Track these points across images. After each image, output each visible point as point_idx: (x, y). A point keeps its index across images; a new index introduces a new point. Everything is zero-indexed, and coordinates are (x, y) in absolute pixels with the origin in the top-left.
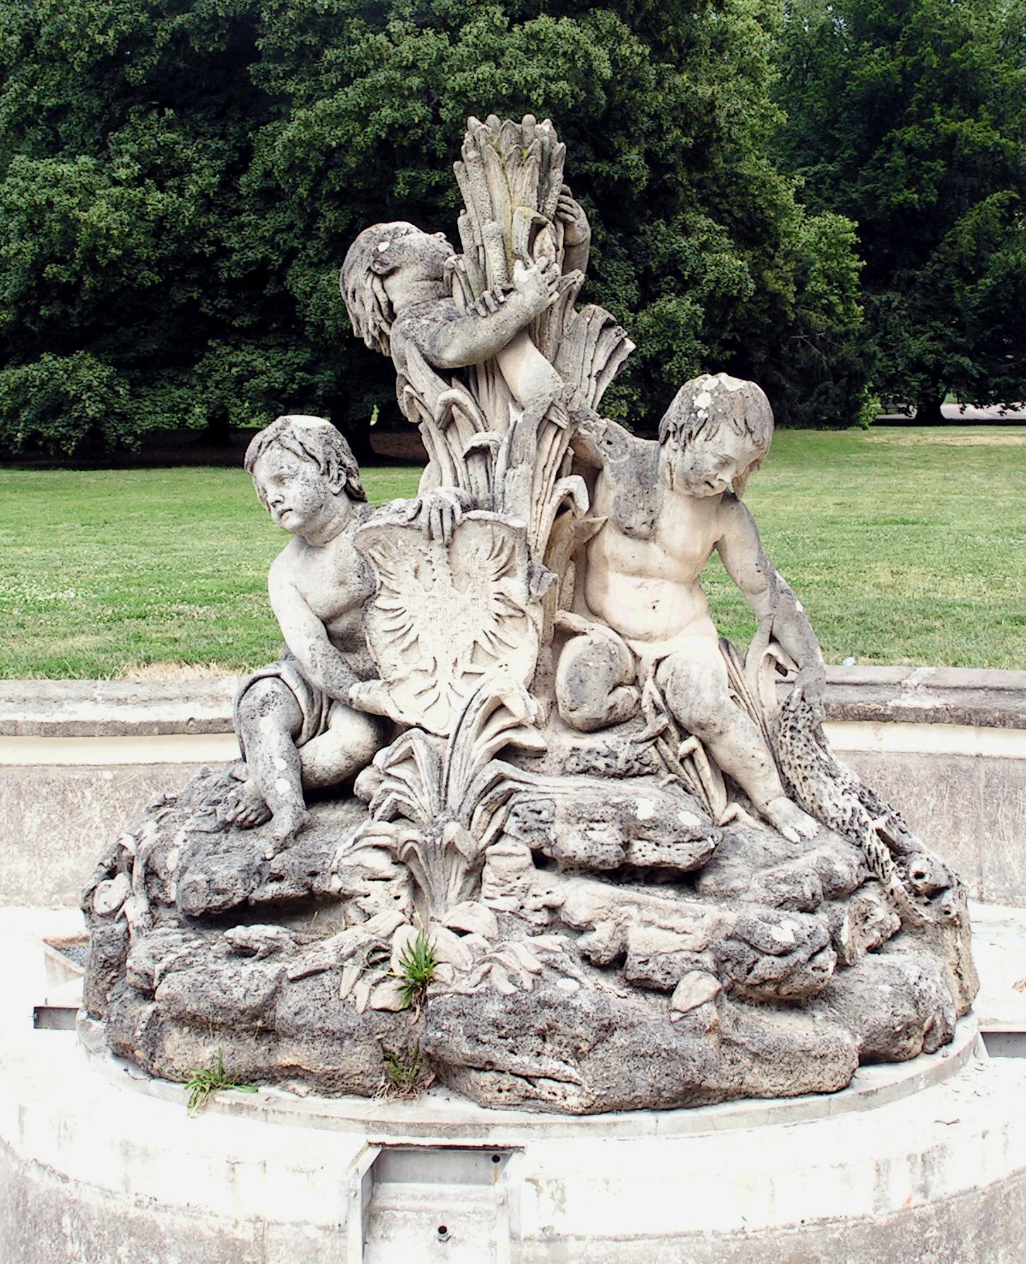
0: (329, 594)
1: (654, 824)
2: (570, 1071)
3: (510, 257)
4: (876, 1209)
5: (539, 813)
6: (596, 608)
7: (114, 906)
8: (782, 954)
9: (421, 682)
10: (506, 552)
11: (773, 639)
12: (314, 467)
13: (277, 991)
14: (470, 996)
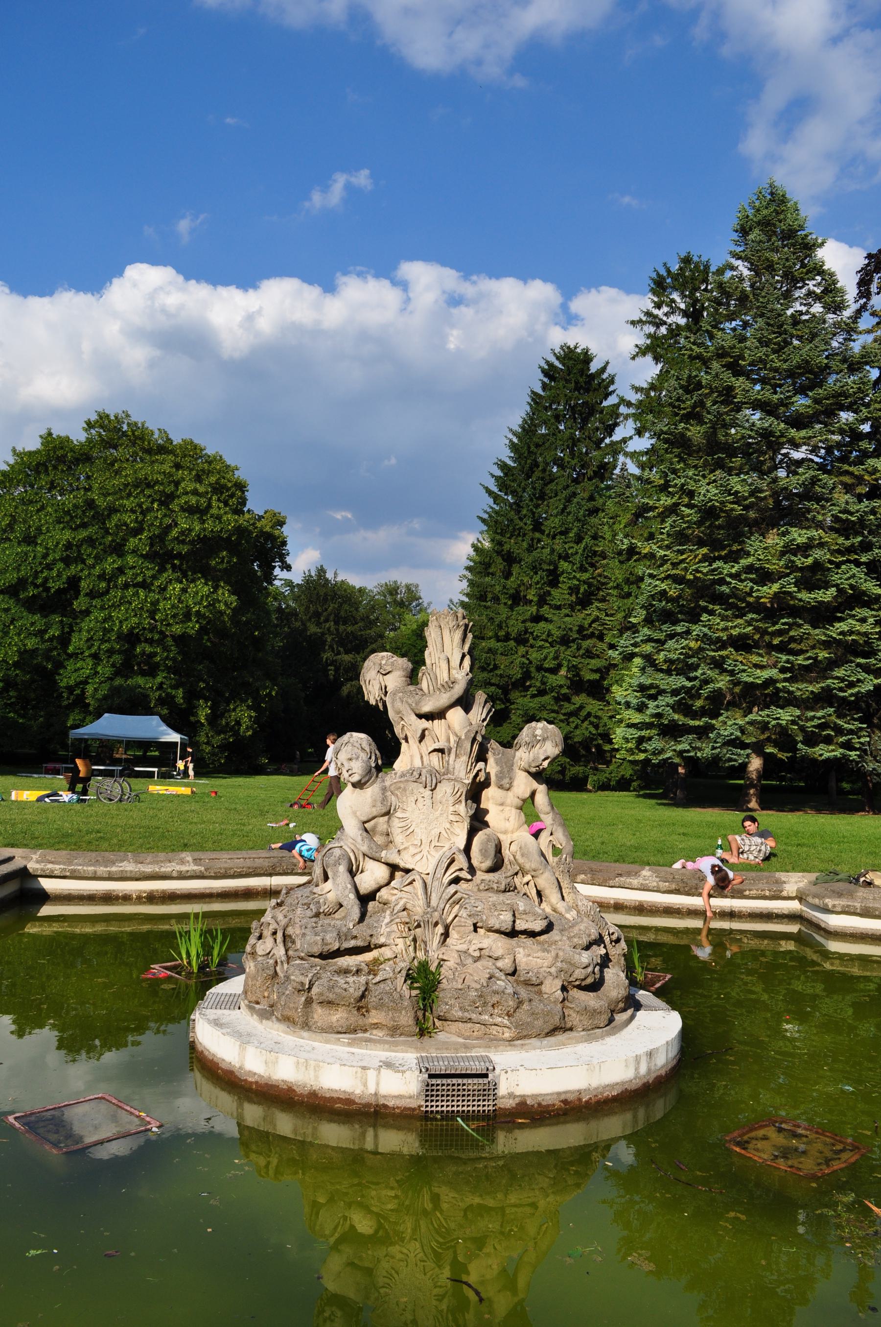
0: (366, 811)
2: (506, 1022)
4: (354, 1143)
9: (412, 850)
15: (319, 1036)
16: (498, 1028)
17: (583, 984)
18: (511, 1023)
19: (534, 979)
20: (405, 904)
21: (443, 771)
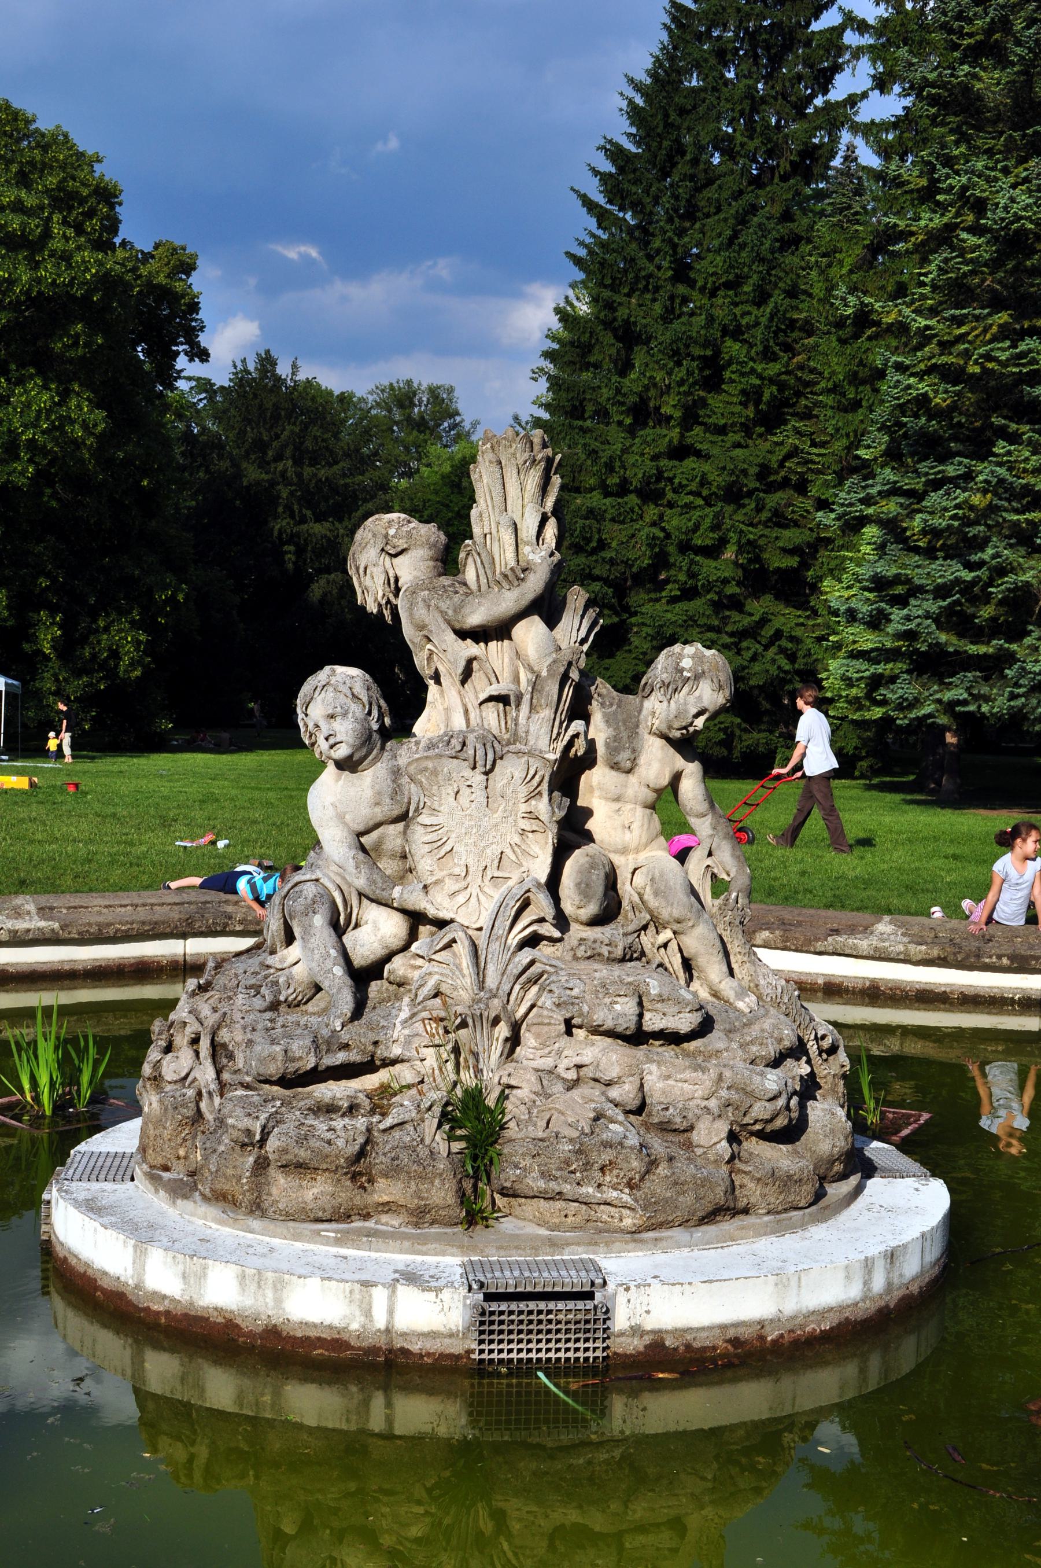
0: (363, 813)
2: (626, 1198)
7: (183, 1074)
8: (770, 1100)
10: (537, 779)
14: (541, 1140)
15: (281, 1227)
17: (769, 1128)
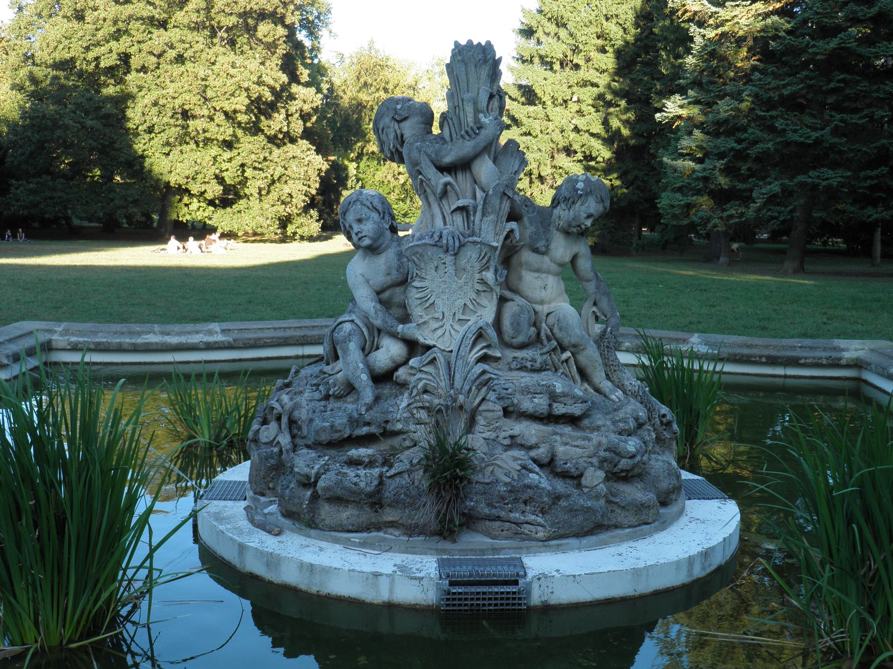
0: (380, 279)
1: (564, 395)
2: (540, 520)
3: (477, 111)
5: (507, 389)
6: (514, 287)
7: (271, 439)
10: (486, 258)
11: (595, 304)
12: (377, 214)
13: (381, 483)
16: (531, 527)
18: (546, 521)
19: (573, 470)
20: (546, 290)
21: (467, 232)
